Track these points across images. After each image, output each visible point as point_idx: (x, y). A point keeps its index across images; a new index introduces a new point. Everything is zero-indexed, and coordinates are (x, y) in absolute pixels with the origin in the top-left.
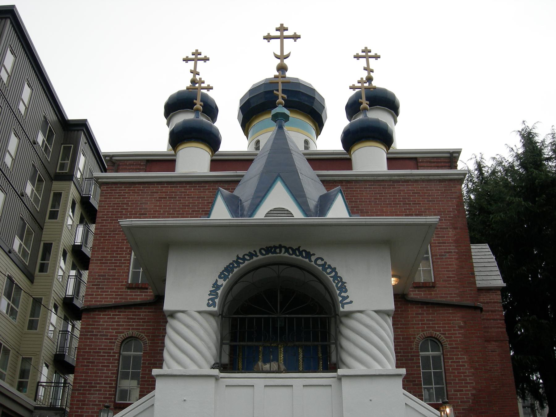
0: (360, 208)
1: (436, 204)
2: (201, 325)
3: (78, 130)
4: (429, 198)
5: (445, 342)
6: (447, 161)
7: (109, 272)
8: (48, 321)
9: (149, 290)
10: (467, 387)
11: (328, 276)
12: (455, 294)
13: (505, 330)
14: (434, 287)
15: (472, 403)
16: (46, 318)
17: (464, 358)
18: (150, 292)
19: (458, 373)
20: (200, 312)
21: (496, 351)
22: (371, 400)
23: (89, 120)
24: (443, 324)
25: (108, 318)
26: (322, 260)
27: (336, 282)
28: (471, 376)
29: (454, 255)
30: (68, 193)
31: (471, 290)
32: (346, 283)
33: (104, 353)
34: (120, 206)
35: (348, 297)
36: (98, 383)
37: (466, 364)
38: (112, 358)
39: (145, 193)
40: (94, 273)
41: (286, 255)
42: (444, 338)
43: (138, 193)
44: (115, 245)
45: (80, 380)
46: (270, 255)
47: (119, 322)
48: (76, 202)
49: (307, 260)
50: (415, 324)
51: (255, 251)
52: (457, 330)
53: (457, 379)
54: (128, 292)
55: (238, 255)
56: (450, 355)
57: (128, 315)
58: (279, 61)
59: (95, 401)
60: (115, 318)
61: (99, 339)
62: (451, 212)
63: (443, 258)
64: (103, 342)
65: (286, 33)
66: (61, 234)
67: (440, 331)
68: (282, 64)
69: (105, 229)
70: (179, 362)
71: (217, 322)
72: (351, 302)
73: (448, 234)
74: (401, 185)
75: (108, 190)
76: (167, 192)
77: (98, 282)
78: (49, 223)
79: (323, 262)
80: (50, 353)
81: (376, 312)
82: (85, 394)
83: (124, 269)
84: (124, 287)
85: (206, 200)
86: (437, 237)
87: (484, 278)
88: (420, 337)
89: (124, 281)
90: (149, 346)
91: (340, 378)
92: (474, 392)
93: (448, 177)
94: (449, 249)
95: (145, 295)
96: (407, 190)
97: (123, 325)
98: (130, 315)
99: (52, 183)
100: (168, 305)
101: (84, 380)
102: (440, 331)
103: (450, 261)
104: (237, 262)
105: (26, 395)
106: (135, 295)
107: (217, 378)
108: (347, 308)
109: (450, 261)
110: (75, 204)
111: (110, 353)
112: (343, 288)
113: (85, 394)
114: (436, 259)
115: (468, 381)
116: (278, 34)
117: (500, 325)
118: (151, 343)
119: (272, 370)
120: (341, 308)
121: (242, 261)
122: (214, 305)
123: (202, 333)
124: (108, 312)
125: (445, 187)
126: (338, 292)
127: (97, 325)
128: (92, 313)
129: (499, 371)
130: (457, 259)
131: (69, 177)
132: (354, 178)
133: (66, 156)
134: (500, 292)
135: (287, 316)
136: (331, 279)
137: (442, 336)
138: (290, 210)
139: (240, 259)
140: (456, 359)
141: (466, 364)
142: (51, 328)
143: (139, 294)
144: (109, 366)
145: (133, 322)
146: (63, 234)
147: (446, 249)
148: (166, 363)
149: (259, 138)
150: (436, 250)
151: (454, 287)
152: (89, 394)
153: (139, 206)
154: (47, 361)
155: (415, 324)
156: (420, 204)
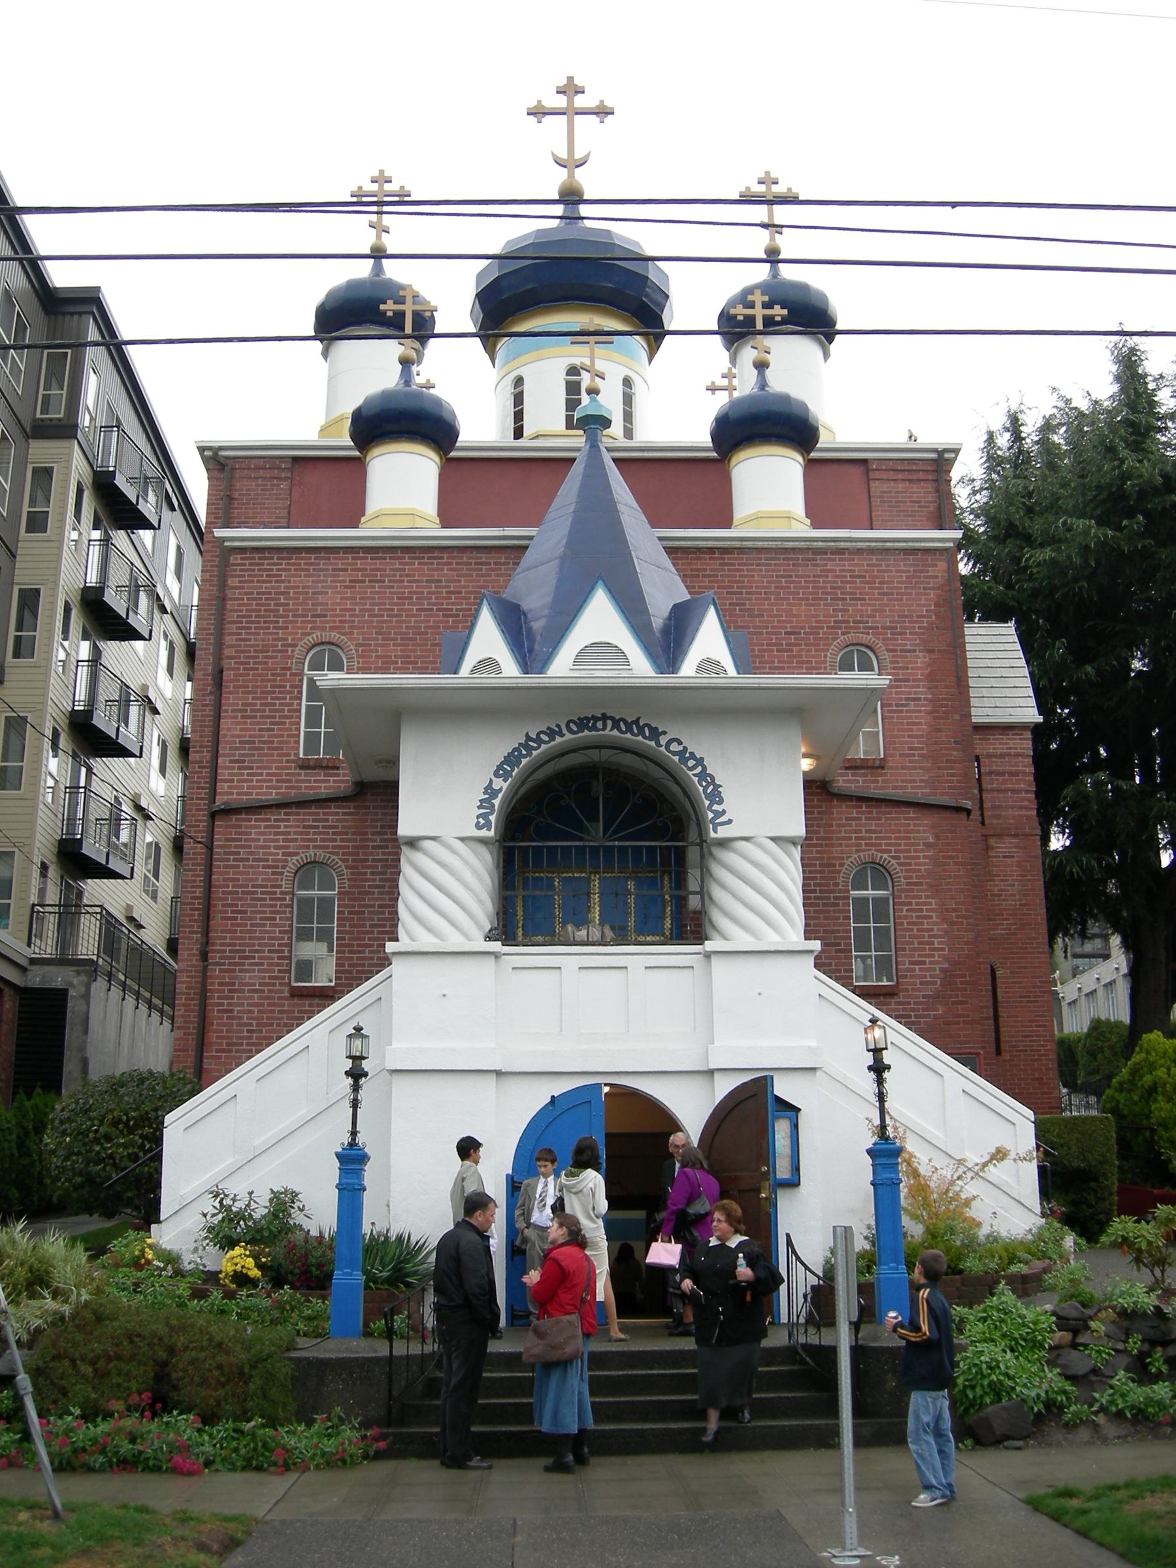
0: (748, 607)
1: (896, 600)
2: (466, 862)
3: (80, 314)
4: (882, 588)
5: (897, 873)
6: (929, 468)
7: (261, 736)
8: (44, 769)
9: (341, 771)
10: (933, 956)
11: (690, 773)
12: (921, 781)
13: (1035, 813)
14: (883, 768)
15: (941, 985)
16: (38, 763)
17: (930, 904)
18: (344, 775)
19: (919, 930)
20: (462, 839)
21: (1013, 857)
22: (760, 994)
23: (103, 289)
24: (896, 838)
25: (266, 827)
26: (680, 743)
27: (704, 784)
29: (923, 705)
30: (68, 468)
31: (952, 775)
32: (721, 786)
33: (262, 893)
34: (273, 599)
35: (724, 812)
36: (257, 951)
38: (279, 903)
39: (321, 570)
40: (232, 736)
41: (615, 732)
42: (896, 866)
43: (308, 570)
44: (268, 680)
45: (222, 945)
46: (586, 733)
47: (289, 833)
48: (85, 488)
49: (653, 743)
50: (844, 838)
51: (558, 726)
52: (922, 851)
54: (300, 774)
55: (527, 733)
56: (906, 897)
57: (304, 820)
58: (562, 174)
59: (254, 985)
60: (279, 827)
61: (252, 867)
62: (923, 616)
63: (902, 711)
65: (580, 101)
66: (58, 569)
67: (890, 851)
68: (571, 183)
69: (245, 646)
70: (430, 929)
71: (491, 853)
72: (730, 822)
73: (916, 662)
74: (830, 560)
75: (245, 565)
76: (366, 570)
77: (240, 755)
78: (28, 543)
79: (681, 748)
80: (49, 837)
81: (773, 839)
82: (233, 971)
83: (291, 729)
84: (293, 765)
85: (445, 587)
86: (894, 668)
87: (999, 703)
88: (851, 862)
89: (293, 752)
90: (349, 880)
91: (708, 956)
92: (946, 965)
93: (923, 544)
94: (915, 693)
95: (334, 781)
96: (841, 571)
97: (296, 840)
98: (308, 820)
100: (405, 828)
102: (890, 851)
103: (916, 718)
104: (525, 746)
105: (10, 934)
106: (315, 781)
107: (496, 956)
108: (723, 832)
109: (916, 718)
110: (83, 491)
111: (275, 893)
112: (716, 796)
113: (233, 971)
114: (889, 711)
115: (936, 946)
116: (561, 102)
117: (1026, 803)
118: (352, 874)
119: (590, 939)
120: (712, 832)
121: (535, 745)
122: (488, 825)
123: (469, 877)
124: (265, 814)
126: (707, 803)
128: (234, 817)
129: (1017, 897)
131: (66, 430)
132: (737, 544)
133: (55, 374)
134: (1029, 733)
135: (616, 843)
136: (696, 779)
137: (893, 861)
138: (620, 646)
140: (917, 904)
141: (934, 915)
142: (51, 783)
143: (322, 778)
144: (275, 919)
145: (315, 833)
146: (63, 568)
147: (910, 693)
148: (404, 927)
149: (522, 372)
151: (921, 768)
152: (240, 971)
153: (311, 599)
154: (45, 857)
155: (844, 838)
156: (864, 599)
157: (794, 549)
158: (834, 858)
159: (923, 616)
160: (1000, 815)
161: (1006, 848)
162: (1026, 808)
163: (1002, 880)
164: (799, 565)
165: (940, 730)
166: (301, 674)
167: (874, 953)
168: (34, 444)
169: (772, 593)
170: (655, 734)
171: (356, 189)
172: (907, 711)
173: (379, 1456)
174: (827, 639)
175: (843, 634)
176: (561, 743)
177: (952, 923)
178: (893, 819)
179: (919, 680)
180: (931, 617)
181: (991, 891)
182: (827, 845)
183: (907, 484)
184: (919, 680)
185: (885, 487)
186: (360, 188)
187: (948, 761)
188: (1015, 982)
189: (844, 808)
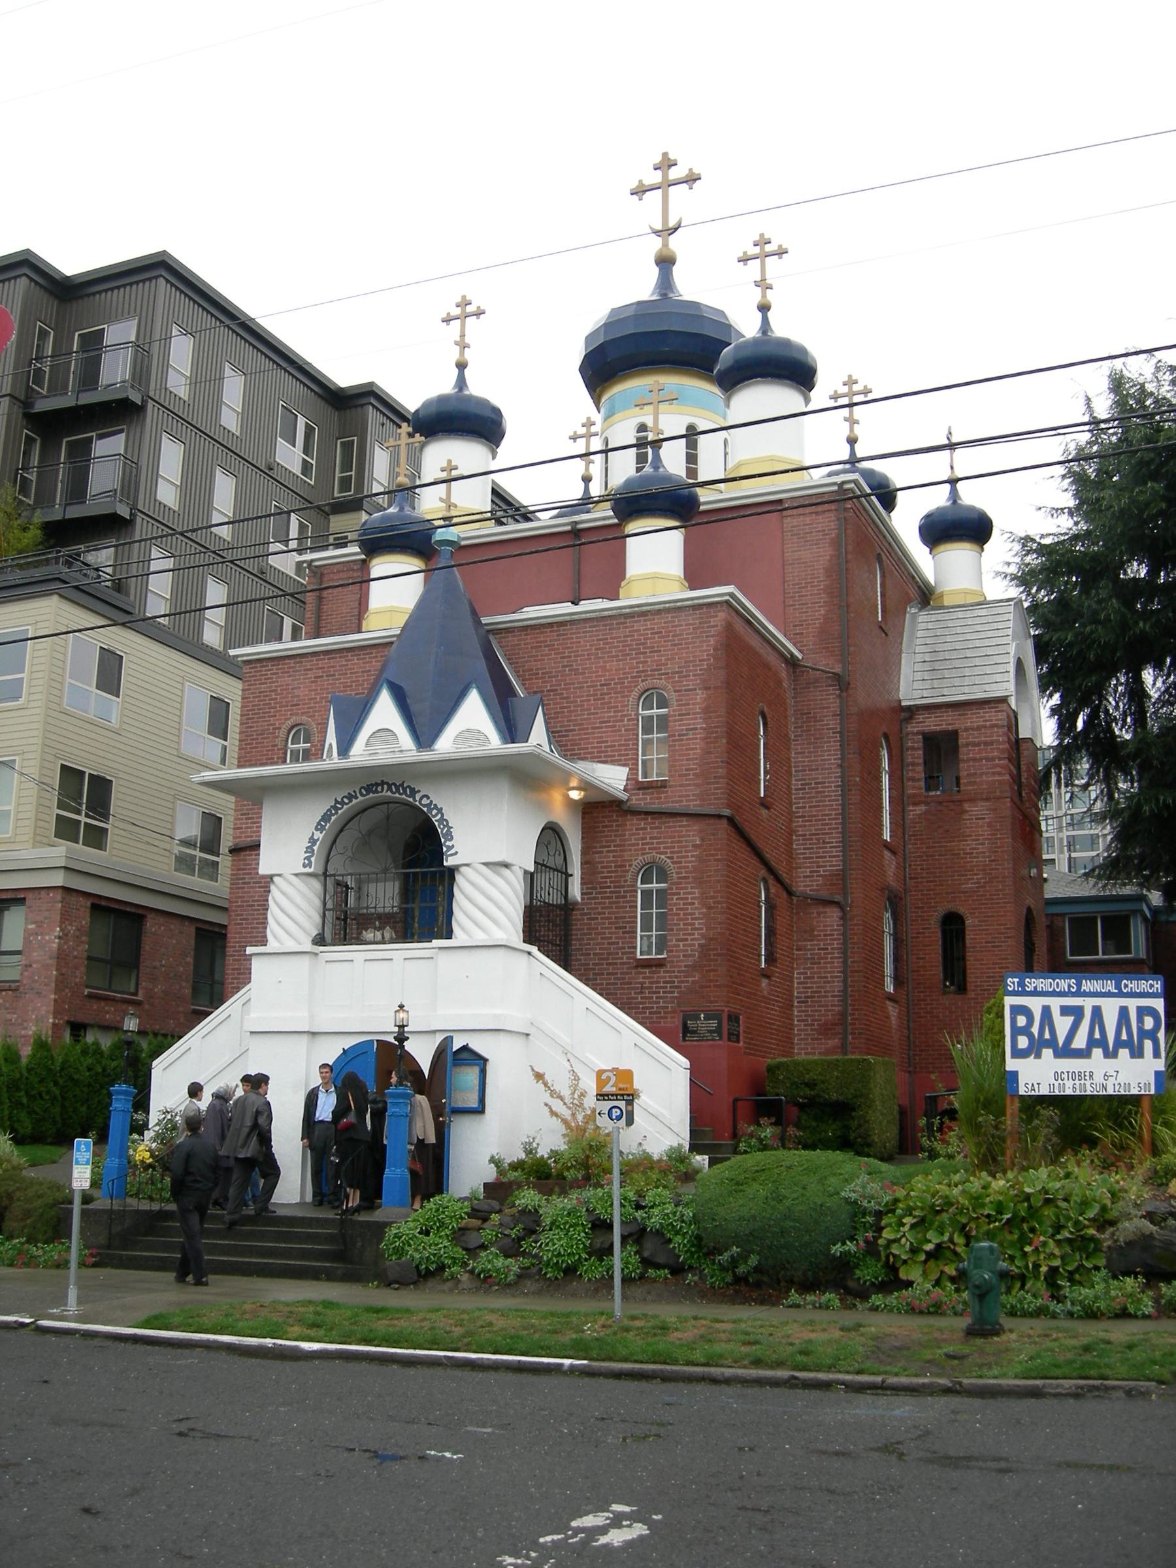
3: (362, 406)
12: (693, 795)
14: (665, 787)
15: (699, 957)
17: (694, 893)
19: (684, 914)
20: (296, 875)
24: (672, 842)
26: (428, 798)
28: (700, 919)
29: (700, 733)
37: (696, 902)
41: (389, 793)
46: (371, 795)
50: (633, 845)
51: (355, 792)
53: (681, 923)
56: (677, 888)
62: (704, 660)
64: (256, 892)
72: (456, 853)
74: (636, 622)
81: (485, 864)
86: (679, 705)
87: (977, 680)
99: (329, 520)
101: (238, 942)
102: (667, 853)
104: (334, 807)
122: (310, 865)
123: (299, 899)
125: (700, 618)
127: (249, 869)
130: (703, 739)
132: (568, 618)
136: (436, 824)
137: (668, 861)
139: (338, 803)
141: (696, 902)
147: (689, 724)
150: (675, 726)
155: (633, 845)
157: (610, 616)
158: (625, 861)
159: (704, 660)
160: (975, 782)
161: (978, 811)
162: (999, 774)
163: (974, 840)
164: (614, 629)
165: (710, 753)
166: (637, 714)
167: (654, 932)
168: (333, 518)
169: (592, 654)
170: (413, 792)
171: (445, 315)
172: (687, 739)
173: (95, 1265)
174: (631, 687)
175: (643, 681)
176: (357, 803)
177: (710, 908)
178: (669, 827)
179: (698, 713)
180: (709, 660)
181: (963, 850)
182: (621, 851)
183: (814, 516)
184: (698, 713)
185: (795, 522)
186: (448, 314)
187: (715, 778)
188: (983, 930)
189: (635, 821)
